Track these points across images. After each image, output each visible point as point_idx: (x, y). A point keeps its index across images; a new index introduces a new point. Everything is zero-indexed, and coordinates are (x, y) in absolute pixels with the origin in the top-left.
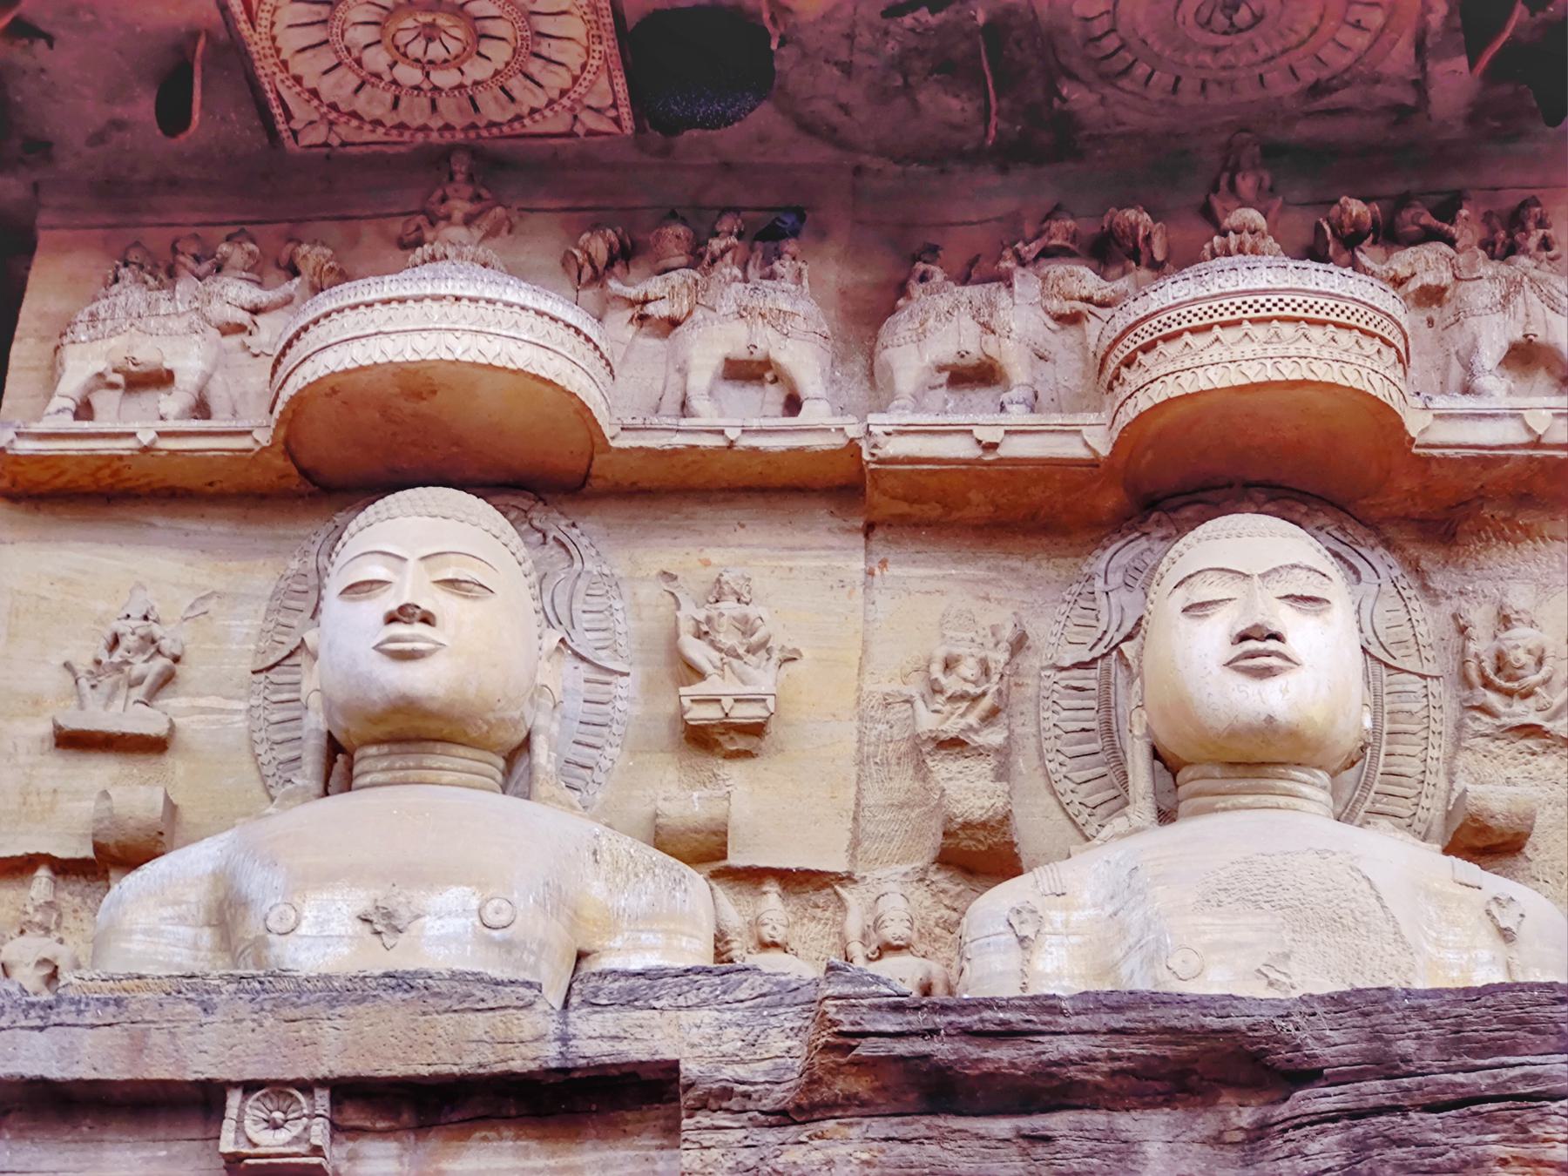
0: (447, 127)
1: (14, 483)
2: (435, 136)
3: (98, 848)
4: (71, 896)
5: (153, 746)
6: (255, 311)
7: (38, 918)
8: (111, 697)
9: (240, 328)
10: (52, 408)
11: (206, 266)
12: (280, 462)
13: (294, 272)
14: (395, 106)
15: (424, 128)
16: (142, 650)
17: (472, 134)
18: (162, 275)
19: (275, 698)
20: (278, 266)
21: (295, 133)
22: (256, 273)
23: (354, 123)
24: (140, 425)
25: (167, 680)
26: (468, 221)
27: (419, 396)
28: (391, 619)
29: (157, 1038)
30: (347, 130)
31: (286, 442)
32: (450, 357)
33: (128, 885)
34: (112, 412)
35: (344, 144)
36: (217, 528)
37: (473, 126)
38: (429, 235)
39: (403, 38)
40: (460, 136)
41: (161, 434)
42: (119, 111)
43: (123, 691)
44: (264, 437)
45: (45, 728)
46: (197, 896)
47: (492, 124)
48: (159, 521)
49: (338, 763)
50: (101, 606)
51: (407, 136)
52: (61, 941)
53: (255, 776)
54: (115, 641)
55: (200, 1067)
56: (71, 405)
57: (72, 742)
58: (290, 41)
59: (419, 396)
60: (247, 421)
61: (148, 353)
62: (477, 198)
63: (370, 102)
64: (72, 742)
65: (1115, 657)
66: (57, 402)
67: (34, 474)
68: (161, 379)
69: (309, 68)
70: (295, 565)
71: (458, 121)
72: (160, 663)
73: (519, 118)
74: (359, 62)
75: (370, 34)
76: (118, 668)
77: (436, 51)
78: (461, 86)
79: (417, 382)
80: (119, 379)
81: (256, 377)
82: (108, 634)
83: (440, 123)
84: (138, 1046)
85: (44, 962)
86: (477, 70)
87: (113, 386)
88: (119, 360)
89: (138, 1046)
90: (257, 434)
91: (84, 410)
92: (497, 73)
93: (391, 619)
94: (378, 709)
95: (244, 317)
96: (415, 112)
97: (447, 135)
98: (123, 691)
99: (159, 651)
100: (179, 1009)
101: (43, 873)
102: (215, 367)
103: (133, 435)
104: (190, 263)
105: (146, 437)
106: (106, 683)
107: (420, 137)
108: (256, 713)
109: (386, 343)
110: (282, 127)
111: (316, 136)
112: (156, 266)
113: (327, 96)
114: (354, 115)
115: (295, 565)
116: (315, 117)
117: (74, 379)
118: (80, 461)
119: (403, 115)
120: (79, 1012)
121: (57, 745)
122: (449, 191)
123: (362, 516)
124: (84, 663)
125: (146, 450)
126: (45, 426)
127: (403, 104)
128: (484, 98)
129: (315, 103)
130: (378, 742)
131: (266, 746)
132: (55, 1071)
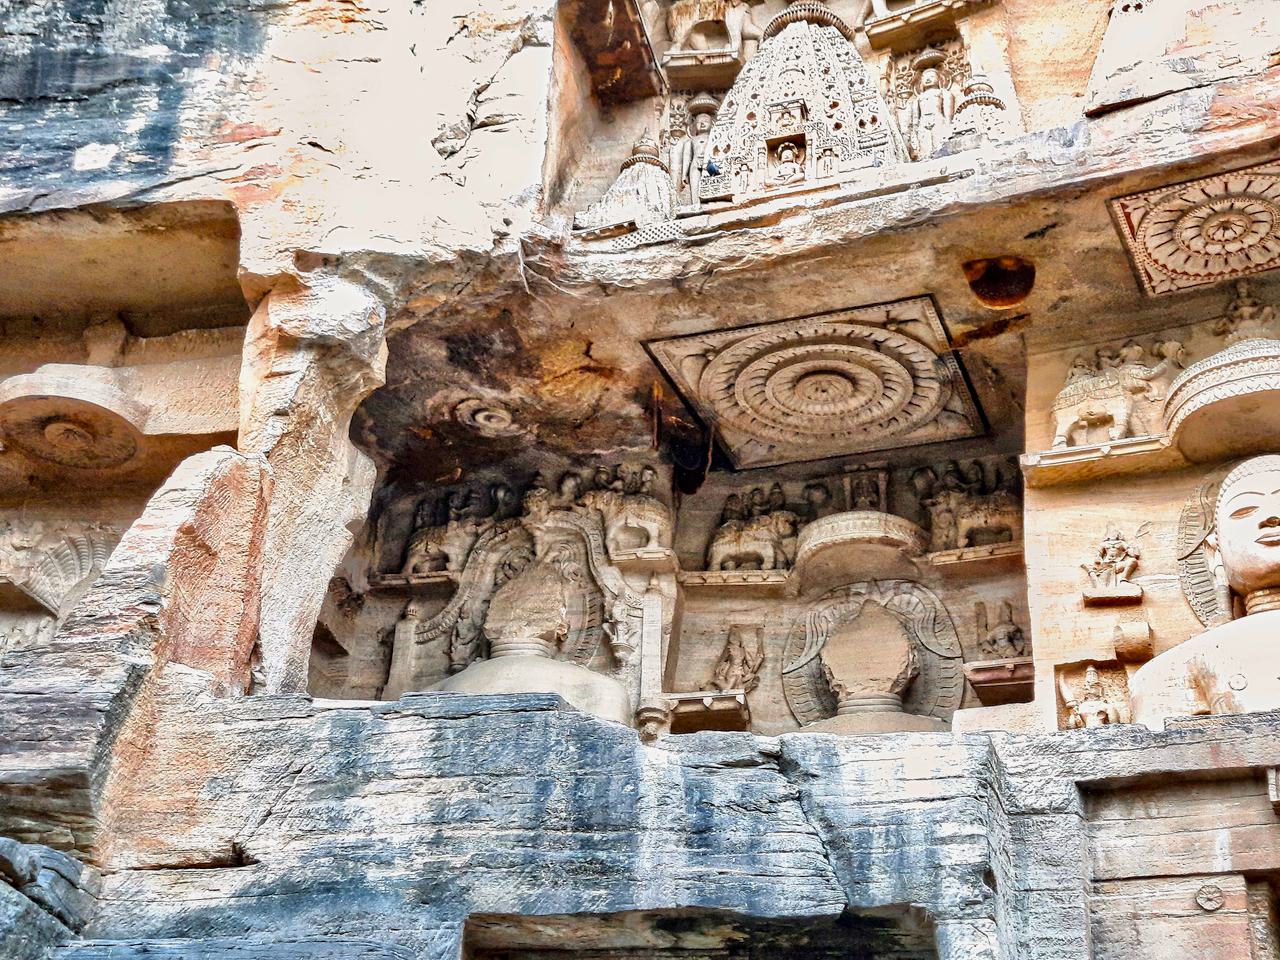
0: (1234, 271)
1: (1040, 480)
2: (1227, 277)
3: (1118, 654)
4: (1106, 679)
5: (1134, 602)
6: (1148, 380)
7: (1093, 691)
8: (1108, 580)
9: (1142, 390)
10: (1056, 442)
11: (1118, 360)
12: (1176, 454)
13: (1161, 357)
14: (1206, 265)
15: (1221, 273)
16: (1118, 555)
17: (1247, 272)
18: (1094, 369)
19: (1194, 571)
20: (1152, 354)
21: (1154, 288)
22: (1142, 361)
23: (1185, 277)
24: (1101, 445)
25: (1134, 568)
26: (1252, 317)
27: (1250, 410)
28: (1263, 525)
29: (1225, 747)
30: (1182, 282)
31: (1178, 443)
32: (1268, 388)
33: (1136, 676)
34: (1083, 440)
35: (1179, 288)
36: (1144, 491)
37: (1248, 268)
38: (1232, 327)
39: (1211, 232)
40: (1240, 274)
41: (1113, 448)
42: (1065, 293)
43: (1113, 576)
44: (1166, 442)
45: (1079, 598)
46: (1183, 673)
47: (1257, 265)
48: (1114, 491)
49: (1238, 601)
50: (1093, 535)
51: (1212, 279)
52: (1106, 702)
53: (1190, 611)
54: (1104, 553)
55: (1251, 760)
56: (1064, 439)
57: (1096, 604)
58: (1152, 243)
59: (1250, 410)
60: (1157, 436)
61: (1098, 408)
62: (1254, 304)
63: (1192, 266)
64: (1096, 604)
65: (717, 15)
66: (1057, 440)
67: (1051, 475)
68: (1106, 421)
69: (1161, 255)
70: (1189, 503)
71: (1239, 267)
72: (1129, 561)
73: (1272, 260)
74: (1188, 247)
75: (1194, 232)
76: (1109, 565)
77: (1229, 234)
78: (1242, 249)
79: (1248, 404)
80: (1084, 423)
81: (1154, 413)
82: (1100, 549)
83: (1230, 269)
84: (1216, 751)
85: (1101, 712)
86: (1251, 240)
87: (1083, 427)
88: (1084, 413)
89: (1216, 751)
90: (1162, 441)
91: (1071, 441)
92: (1262, 239)
93: (1263, 525)
94: (1263, 572)
95: (1142, 383)
96: (1216, 267)
97: (1234, 275)
98: (1113, 576)
99: (1127, 555)
100: (1233, 732)
101: (1090, 669)
102: (1133, 410)
103: (1098, 450)
104: (1109, 361)
105: (1106, 450)
106: (1104, 575)
107: (1219, 278)
108: (1184, 580)
109: (1232, 386)
110: (1147, 286)
111: (1165, 287)
112: (1090, 365)
113: (1170, 267)
114: (1185, 273)
115: (1189, 503)
116: (1164, 278)
117: (1063, 428)
118: (1073, 466)
119: (1210, 269)
120: (1182, 737)
121: (1086, 606)
122: (1239, 303)
123: (1231, 475)
124: (1090, 562)
125: (1107, 456)
126: (1056, 450)
127: (1210, 263)
128: (1253, 253)
129: (1165, 271)
130: (1262, 589)
131: (1192, 596)
132: (1176, 767)
